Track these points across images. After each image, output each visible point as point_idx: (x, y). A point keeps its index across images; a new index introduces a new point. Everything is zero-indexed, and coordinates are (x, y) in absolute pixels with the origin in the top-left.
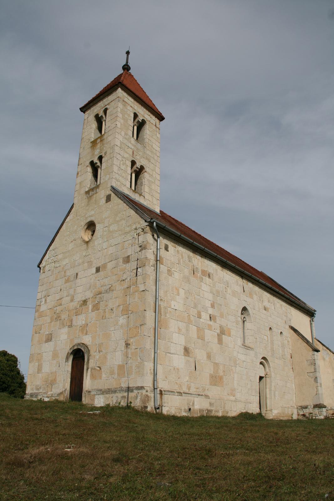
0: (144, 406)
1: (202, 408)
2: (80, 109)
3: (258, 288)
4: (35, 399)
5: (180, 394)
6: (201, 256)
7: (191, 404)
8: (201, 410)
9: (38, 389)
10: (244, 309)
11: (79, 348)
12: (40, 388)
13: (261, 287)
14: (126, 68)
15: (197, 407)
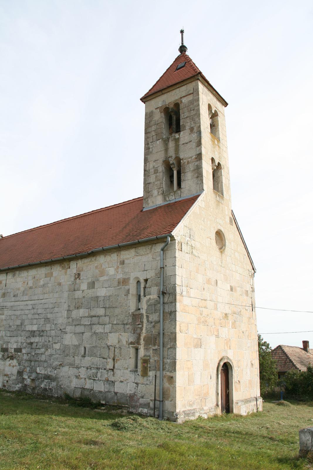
2: (141, 99)
4: (192, 418)
9: (191, 405)
11: (228, 362)
12: (193, 403)
14: (183, 49)
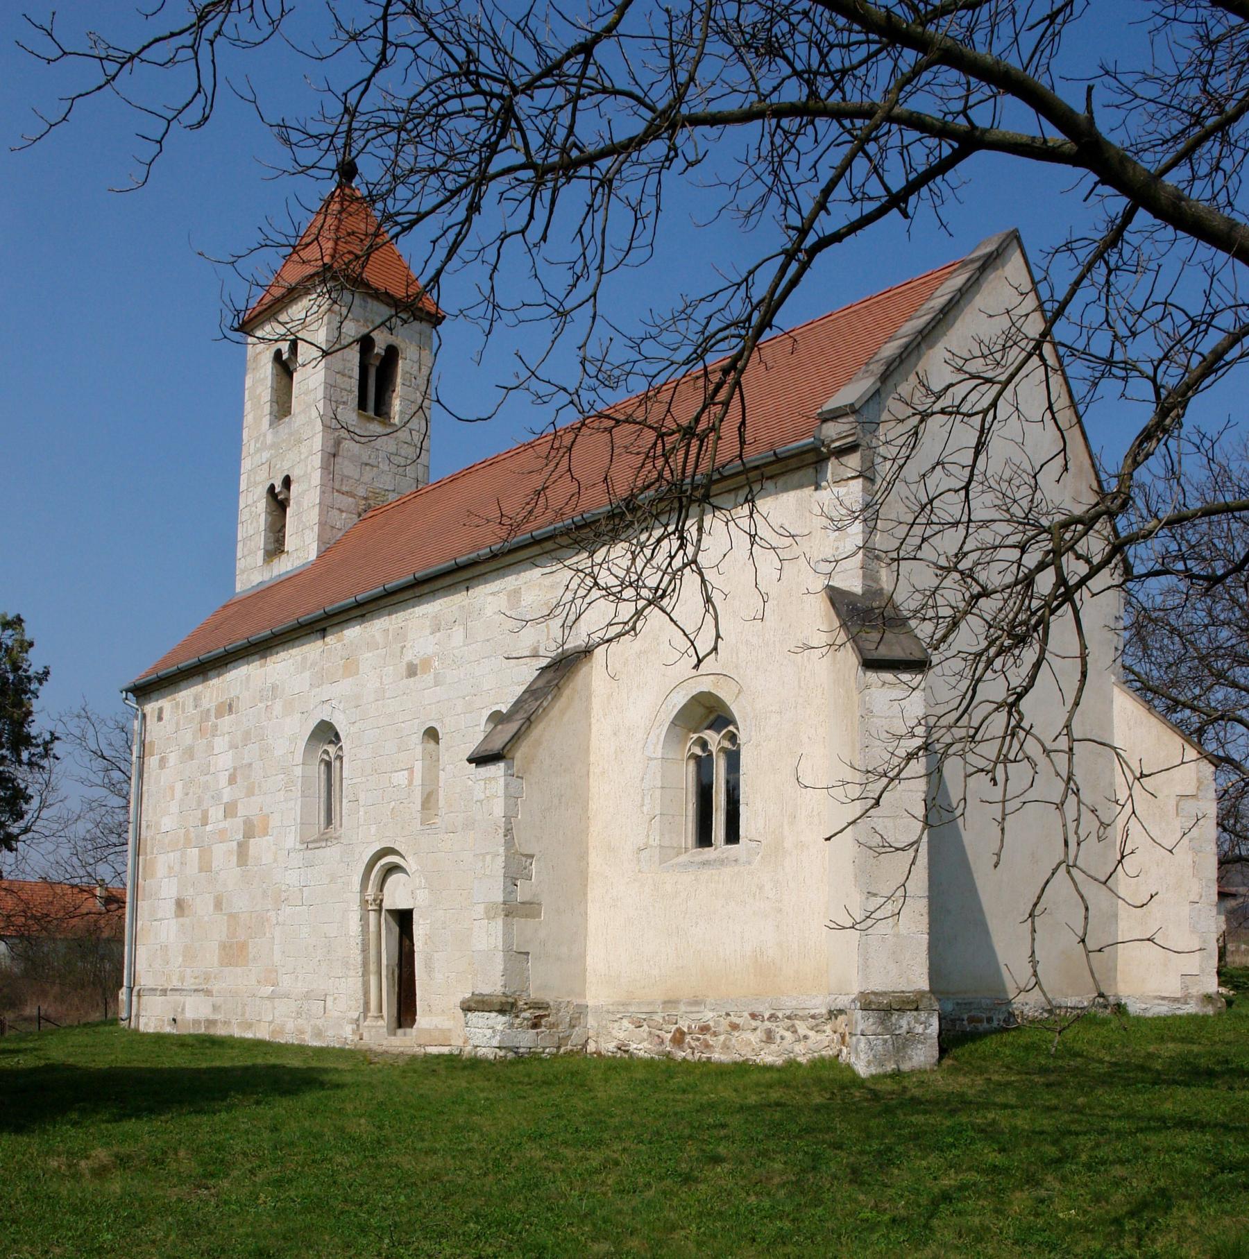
0: (1038, 1184)
1: (196, 1017)
3: (514, 577)
5: (164, 992)
6: (201, 678)
7: (180, 1010)
8: (196, 1022)
10: (326, 733)
13: (297, 638)
15: (190, 1015)
